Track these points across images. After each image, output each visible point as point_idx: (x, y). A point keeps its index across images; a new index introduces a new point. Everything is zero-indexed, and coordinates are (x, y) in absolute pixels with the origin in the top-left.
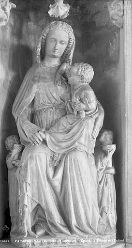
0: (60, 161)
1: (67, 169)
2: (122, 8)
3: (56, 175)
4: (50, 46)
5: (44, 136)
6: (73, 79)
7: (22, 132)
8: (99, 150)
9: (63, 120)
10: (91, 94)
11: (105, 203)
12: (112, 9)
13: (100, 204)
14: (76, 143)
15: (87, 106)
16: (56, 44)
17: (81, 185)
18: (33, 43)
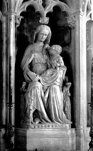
0: (47, 90)
1: (51, 93)
2: (74, 20)
3: (46, 95)
4: (40, 36)
5: (39, 78)
6: (52, 52)
7: (27, 76)
8: (64, 84)
9: (41, 71)
10: (61, 58)
11: (66, 109)
12: (69, 20)
13: (64, 111)
14: (55, 81)
15: (60, 65)
16: (43, 36)
17: (57, 100)
18: (26, 33)
